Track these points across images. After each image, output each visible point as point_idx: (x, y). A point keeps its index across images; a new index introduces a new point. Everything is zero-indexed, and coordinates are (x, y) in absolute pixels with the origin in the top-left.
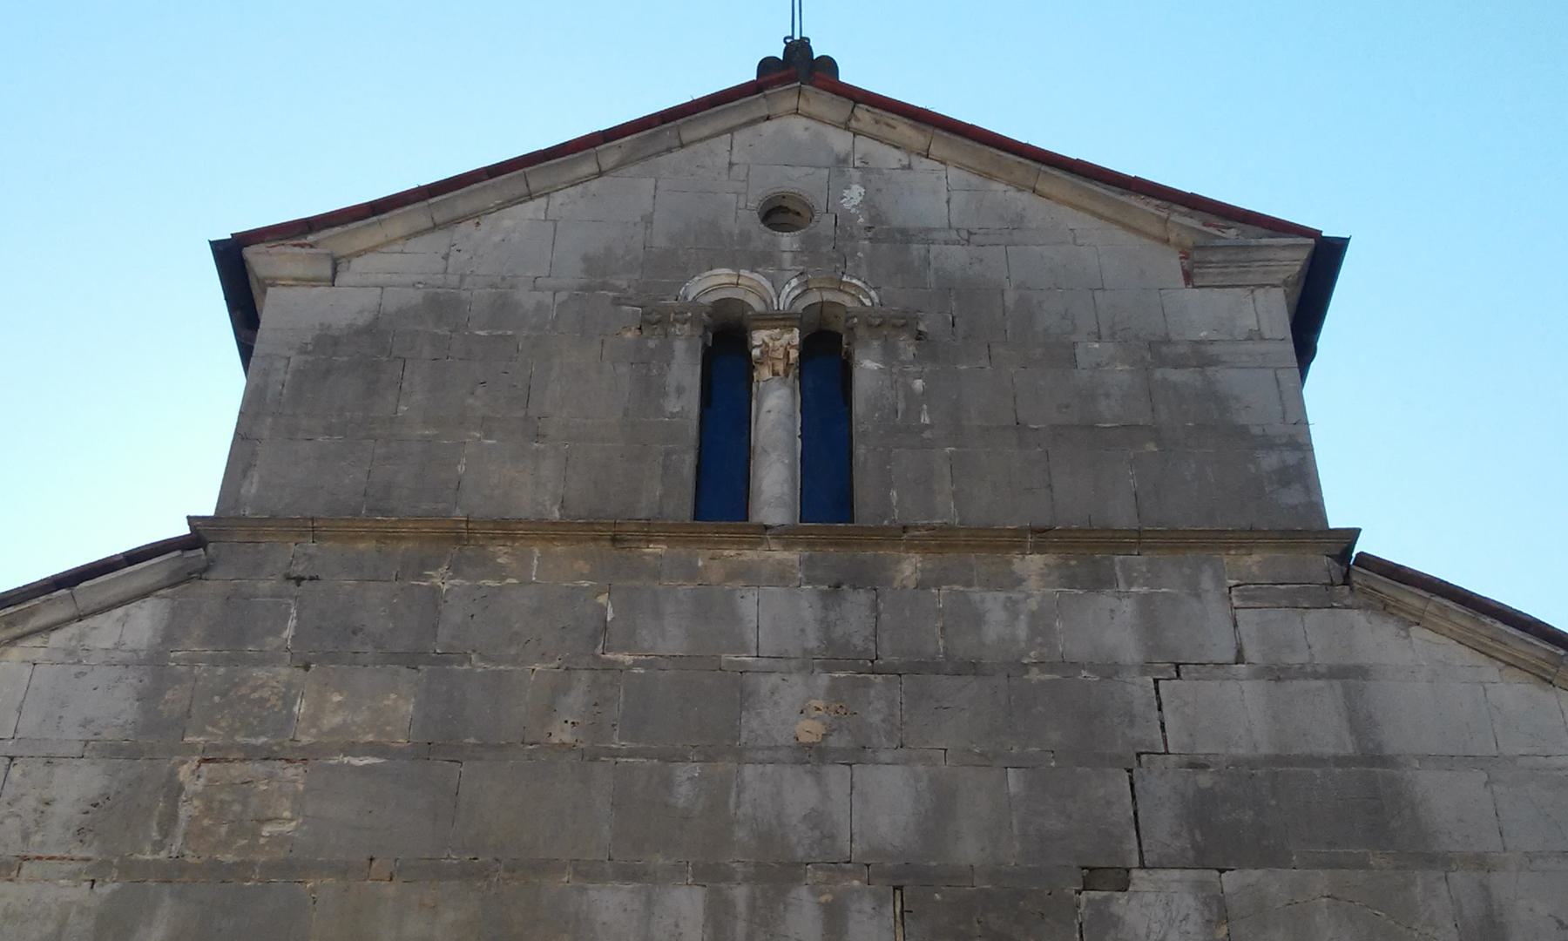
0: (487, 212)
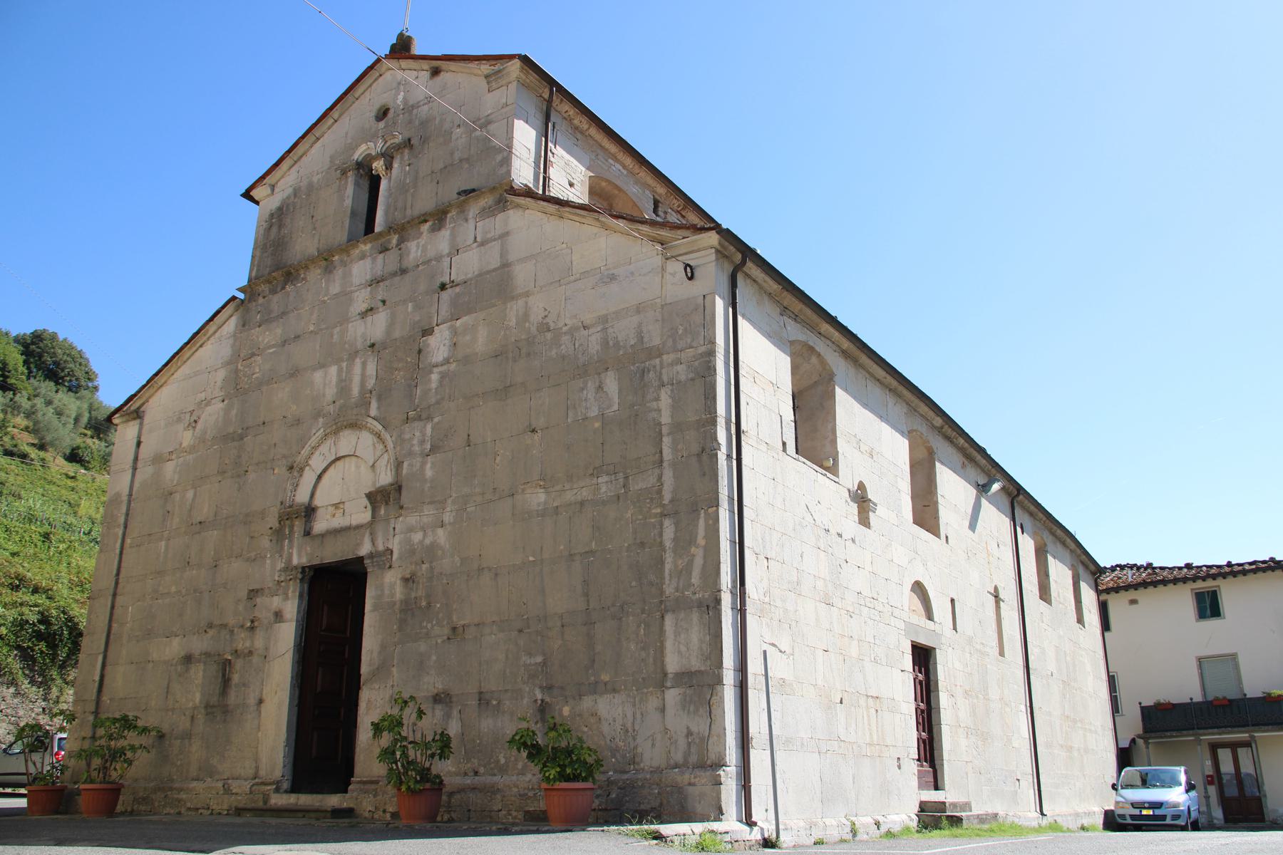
0: (308, 150)
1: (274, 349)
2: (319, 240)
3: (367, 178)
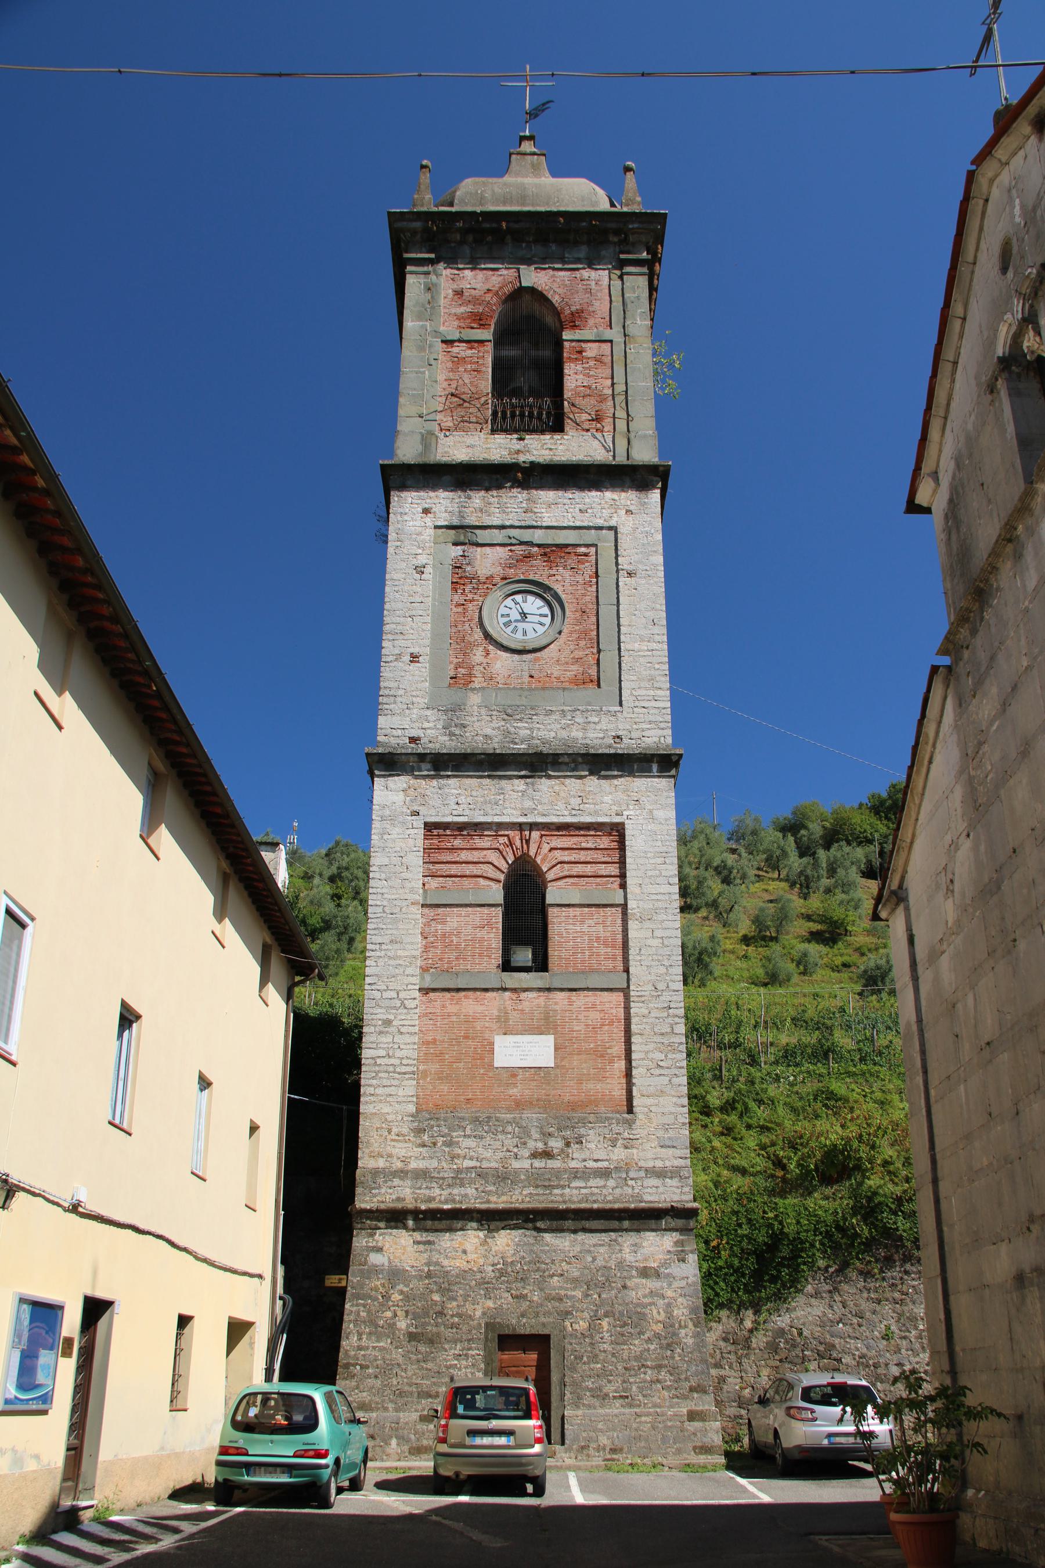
1: (997, 723)
2: (999, 515)
3: (1032, 374)
